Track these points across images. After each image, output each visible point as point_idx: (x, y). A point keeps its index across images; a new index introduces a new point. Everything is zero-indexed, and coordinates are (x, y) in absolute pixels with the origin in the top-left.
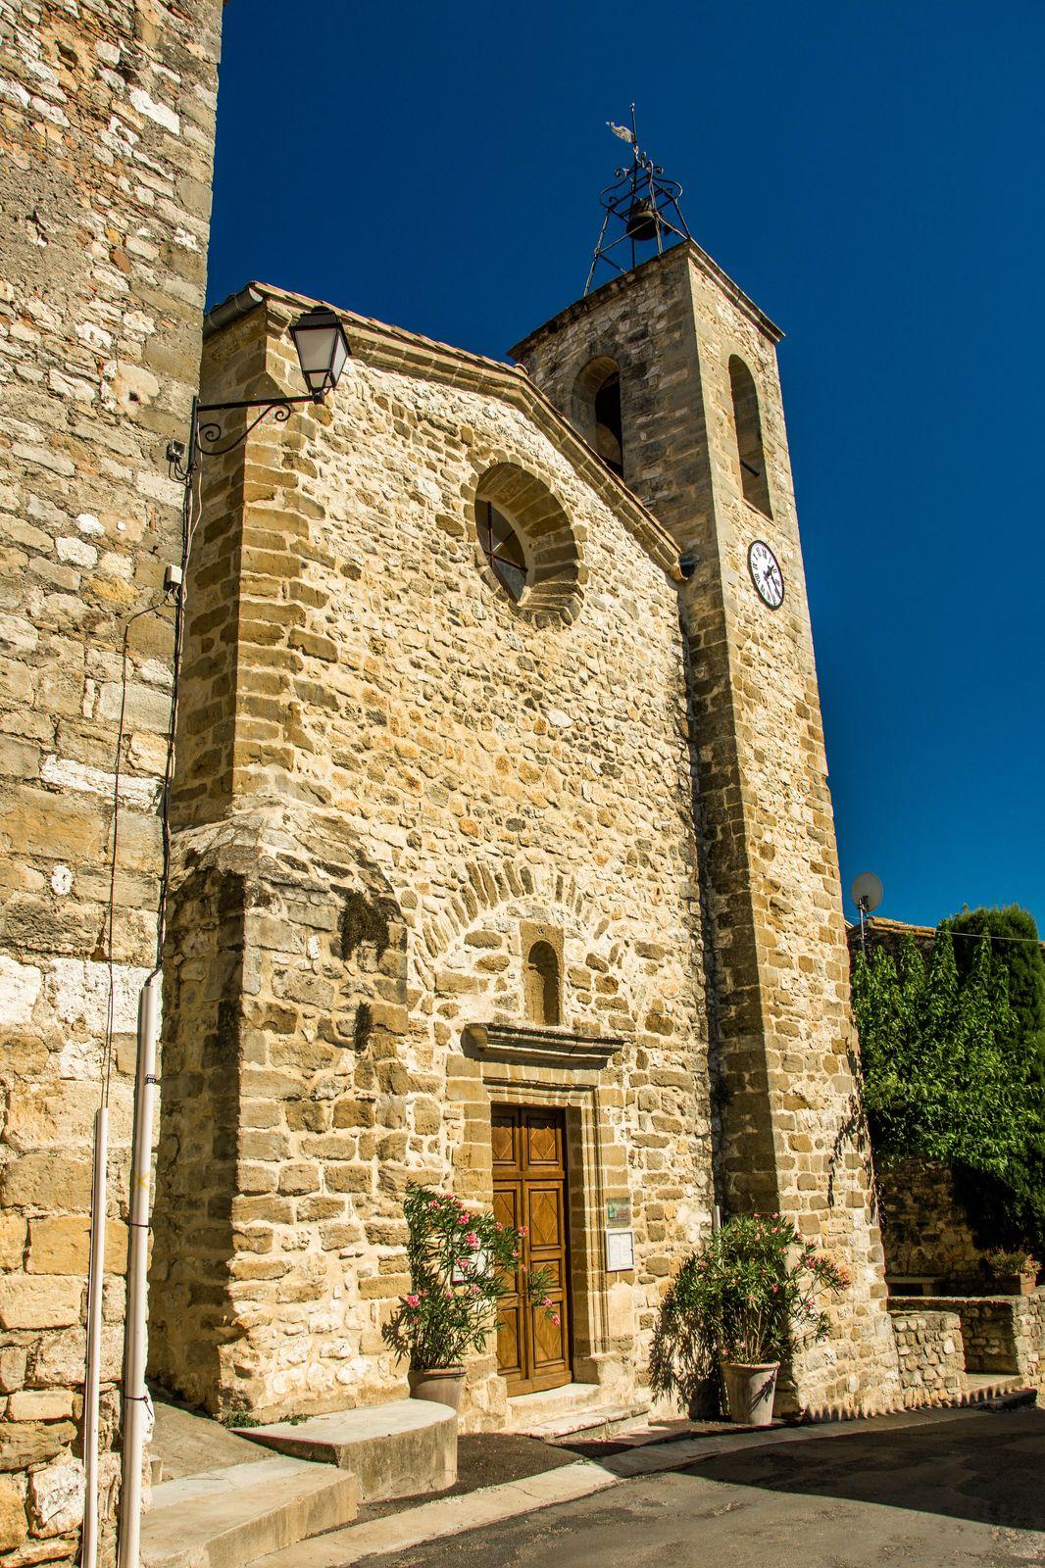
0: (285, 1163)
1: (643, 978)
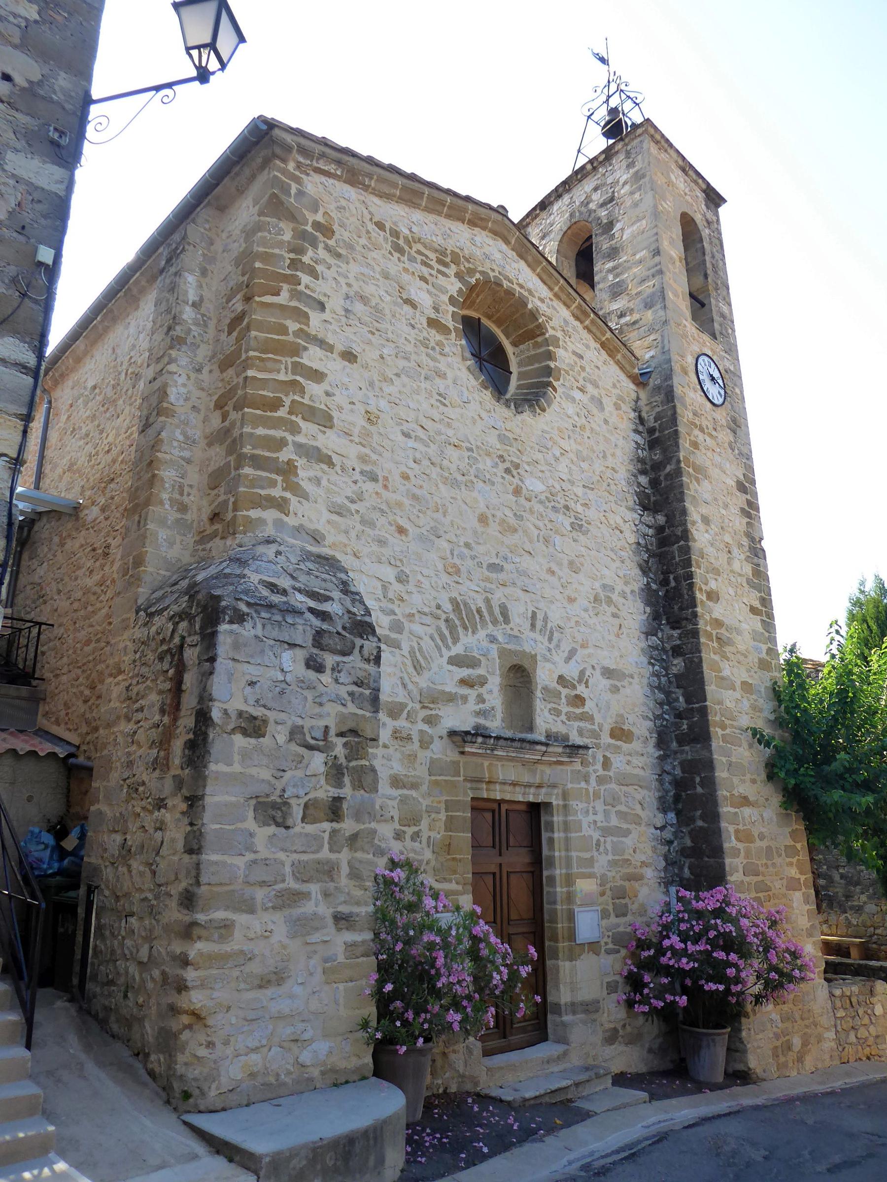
0: (250, 856)
1: (608, 696)
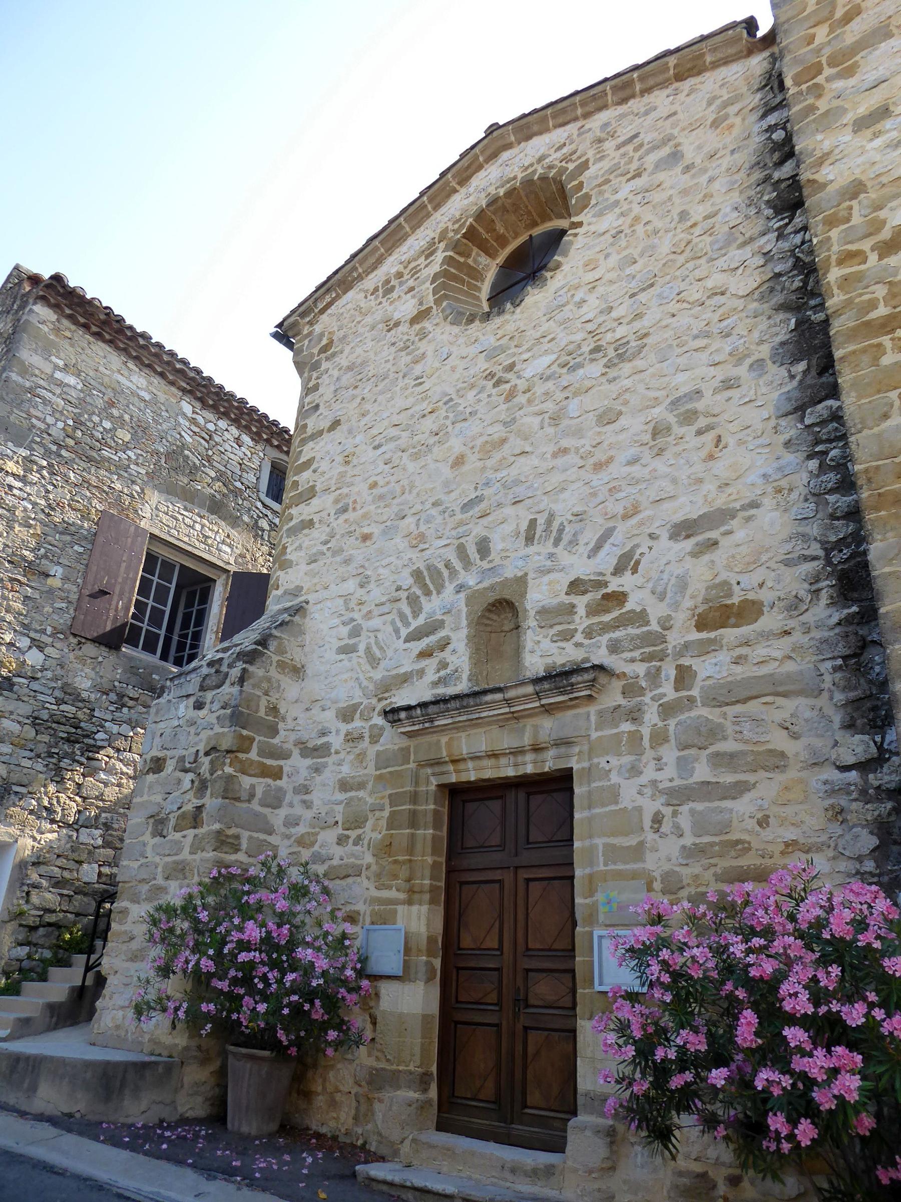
0: (143, 861)
